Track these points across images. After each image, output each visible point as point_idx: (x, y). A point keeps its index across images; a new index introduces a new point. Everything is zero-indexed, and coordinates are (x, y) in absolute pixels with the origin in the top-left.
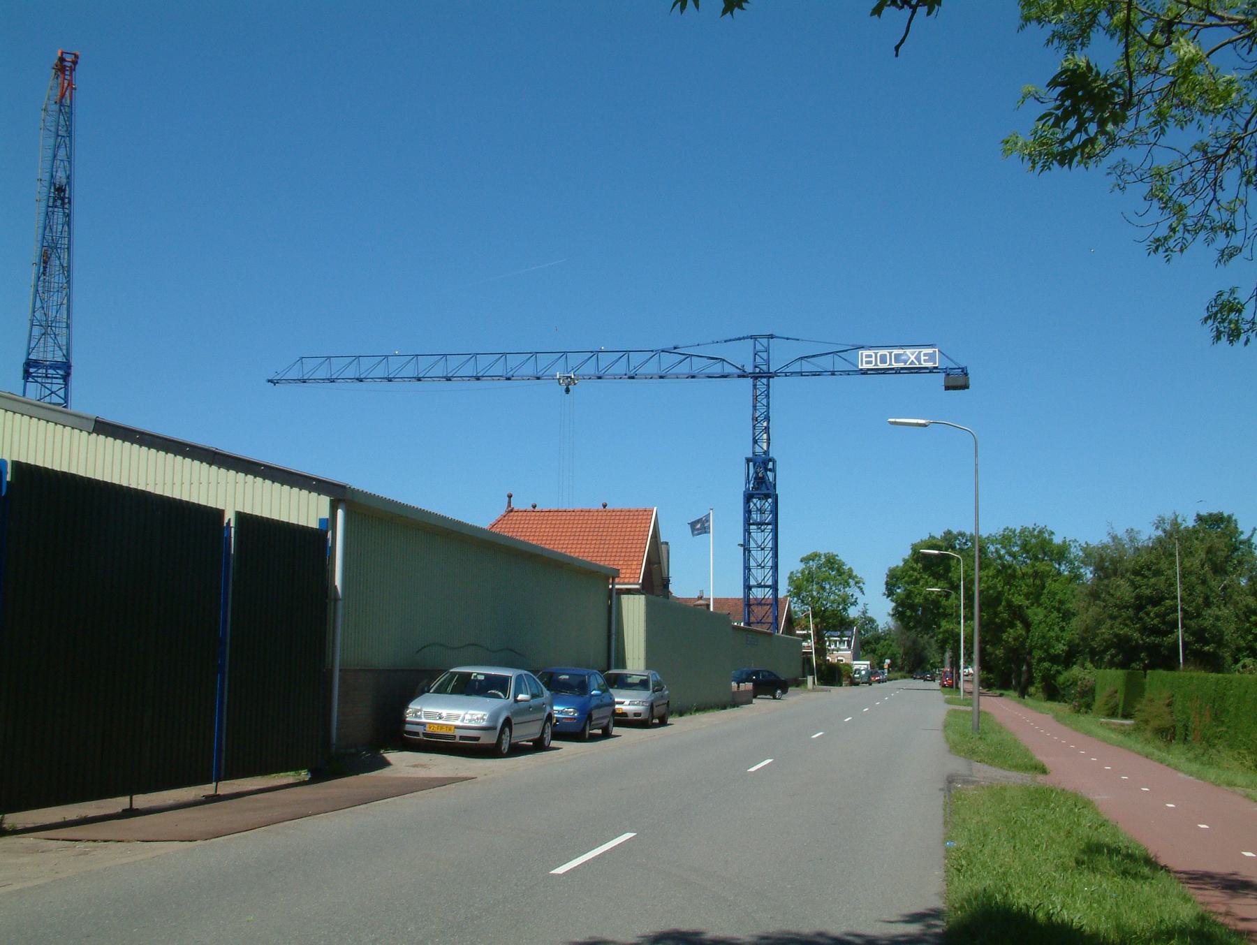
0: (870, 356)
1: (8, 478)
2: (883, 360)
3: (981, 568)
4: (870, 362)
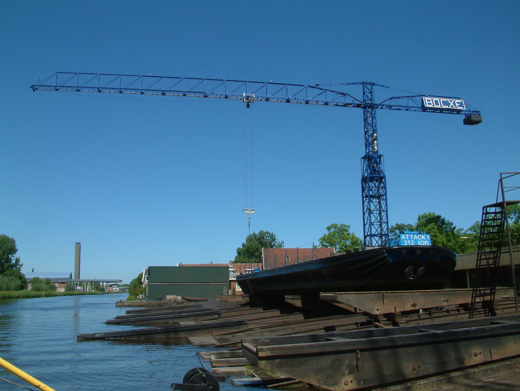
0: (429, 101)
1: (179, 298)
2: (437, 103)
3: (484, 302)
4: (430, 104)
